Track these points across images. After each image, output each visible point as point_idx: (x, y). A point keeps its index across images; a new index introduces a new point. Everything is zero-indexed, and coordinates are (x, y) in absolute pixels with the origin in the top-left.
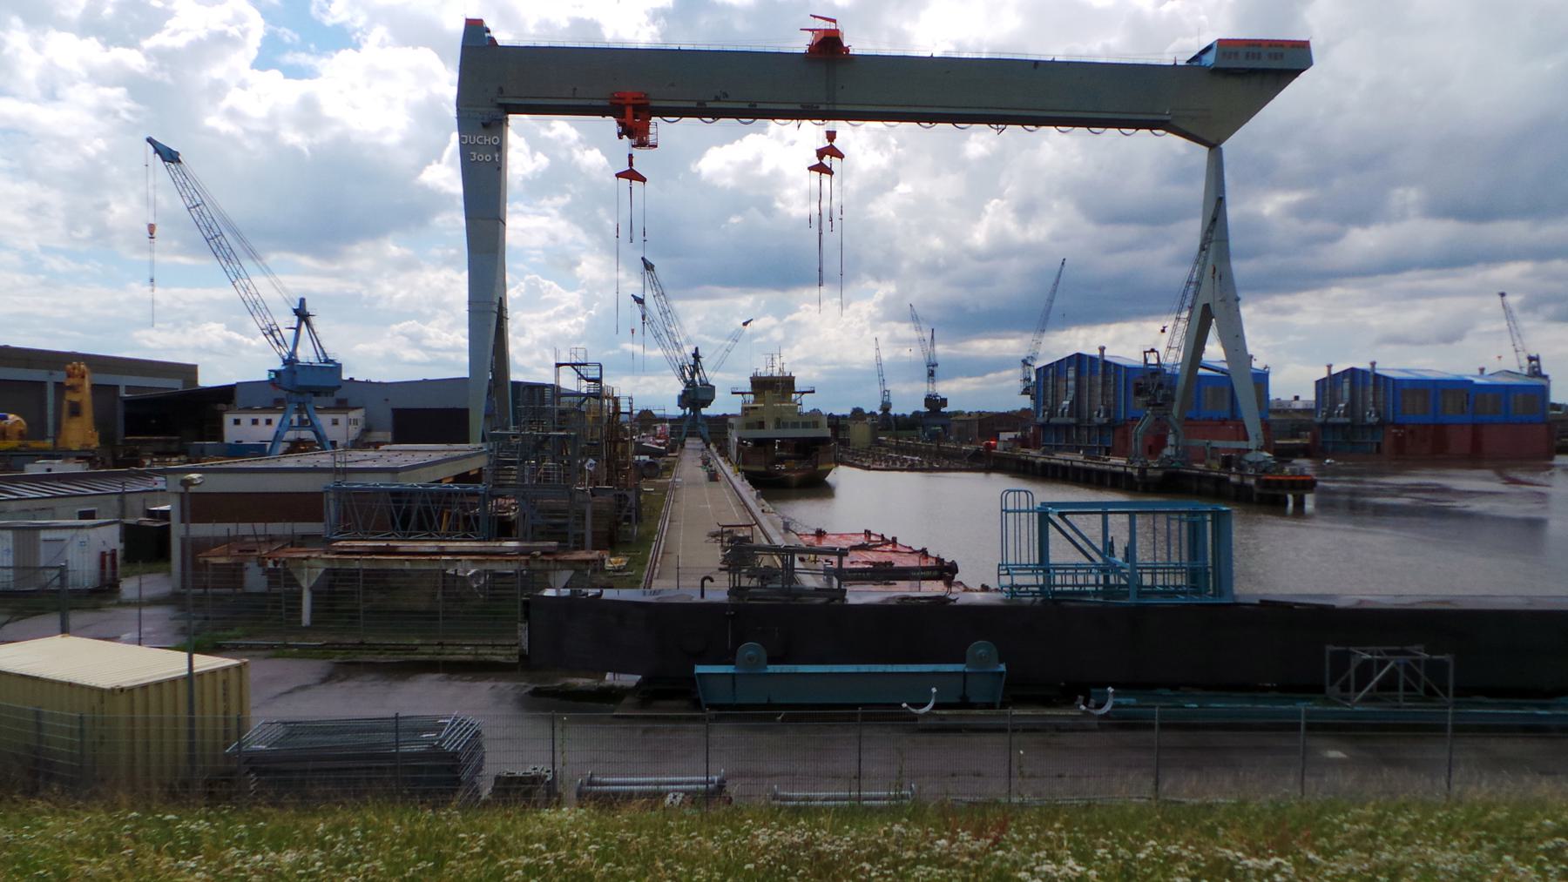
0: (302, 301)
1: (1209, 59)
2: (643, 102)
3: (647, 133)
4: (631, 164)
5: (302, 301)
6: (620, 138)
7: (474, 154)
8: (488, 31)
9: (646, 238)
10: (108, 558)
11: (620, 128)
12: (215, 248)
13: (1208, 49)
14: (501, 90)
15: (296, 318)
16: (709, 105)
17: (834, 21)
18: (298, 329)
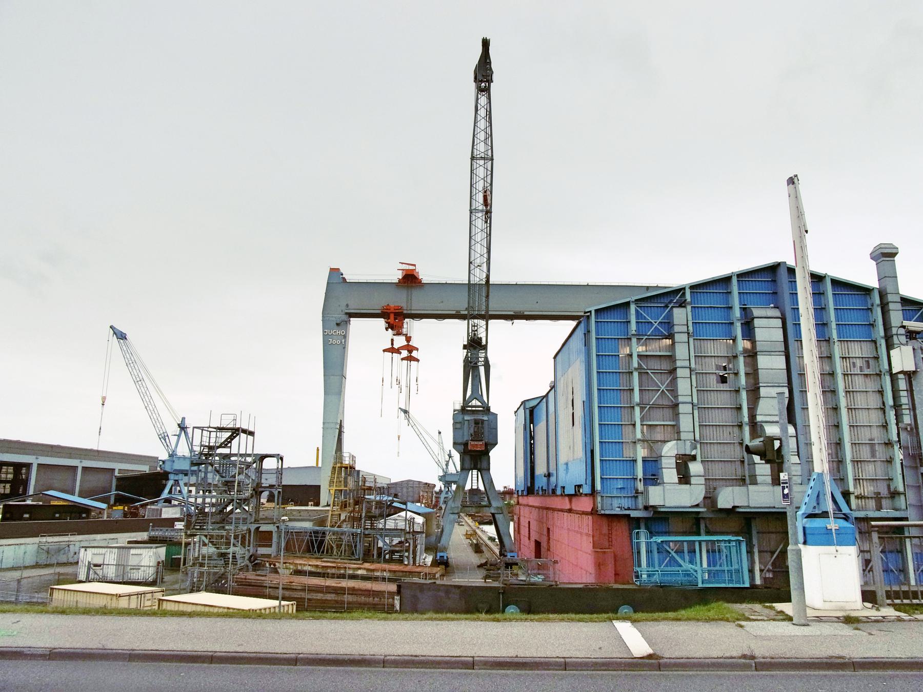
0: (183, 419)
2: (400, 311)
3: (402, 327)
4: (392, 344)
5: (183, 419)
6: (387, 330)
8: (342, 274)
12: (138, 387)
14: (347, 305)
15: (179, 429)
18: (179, 436)
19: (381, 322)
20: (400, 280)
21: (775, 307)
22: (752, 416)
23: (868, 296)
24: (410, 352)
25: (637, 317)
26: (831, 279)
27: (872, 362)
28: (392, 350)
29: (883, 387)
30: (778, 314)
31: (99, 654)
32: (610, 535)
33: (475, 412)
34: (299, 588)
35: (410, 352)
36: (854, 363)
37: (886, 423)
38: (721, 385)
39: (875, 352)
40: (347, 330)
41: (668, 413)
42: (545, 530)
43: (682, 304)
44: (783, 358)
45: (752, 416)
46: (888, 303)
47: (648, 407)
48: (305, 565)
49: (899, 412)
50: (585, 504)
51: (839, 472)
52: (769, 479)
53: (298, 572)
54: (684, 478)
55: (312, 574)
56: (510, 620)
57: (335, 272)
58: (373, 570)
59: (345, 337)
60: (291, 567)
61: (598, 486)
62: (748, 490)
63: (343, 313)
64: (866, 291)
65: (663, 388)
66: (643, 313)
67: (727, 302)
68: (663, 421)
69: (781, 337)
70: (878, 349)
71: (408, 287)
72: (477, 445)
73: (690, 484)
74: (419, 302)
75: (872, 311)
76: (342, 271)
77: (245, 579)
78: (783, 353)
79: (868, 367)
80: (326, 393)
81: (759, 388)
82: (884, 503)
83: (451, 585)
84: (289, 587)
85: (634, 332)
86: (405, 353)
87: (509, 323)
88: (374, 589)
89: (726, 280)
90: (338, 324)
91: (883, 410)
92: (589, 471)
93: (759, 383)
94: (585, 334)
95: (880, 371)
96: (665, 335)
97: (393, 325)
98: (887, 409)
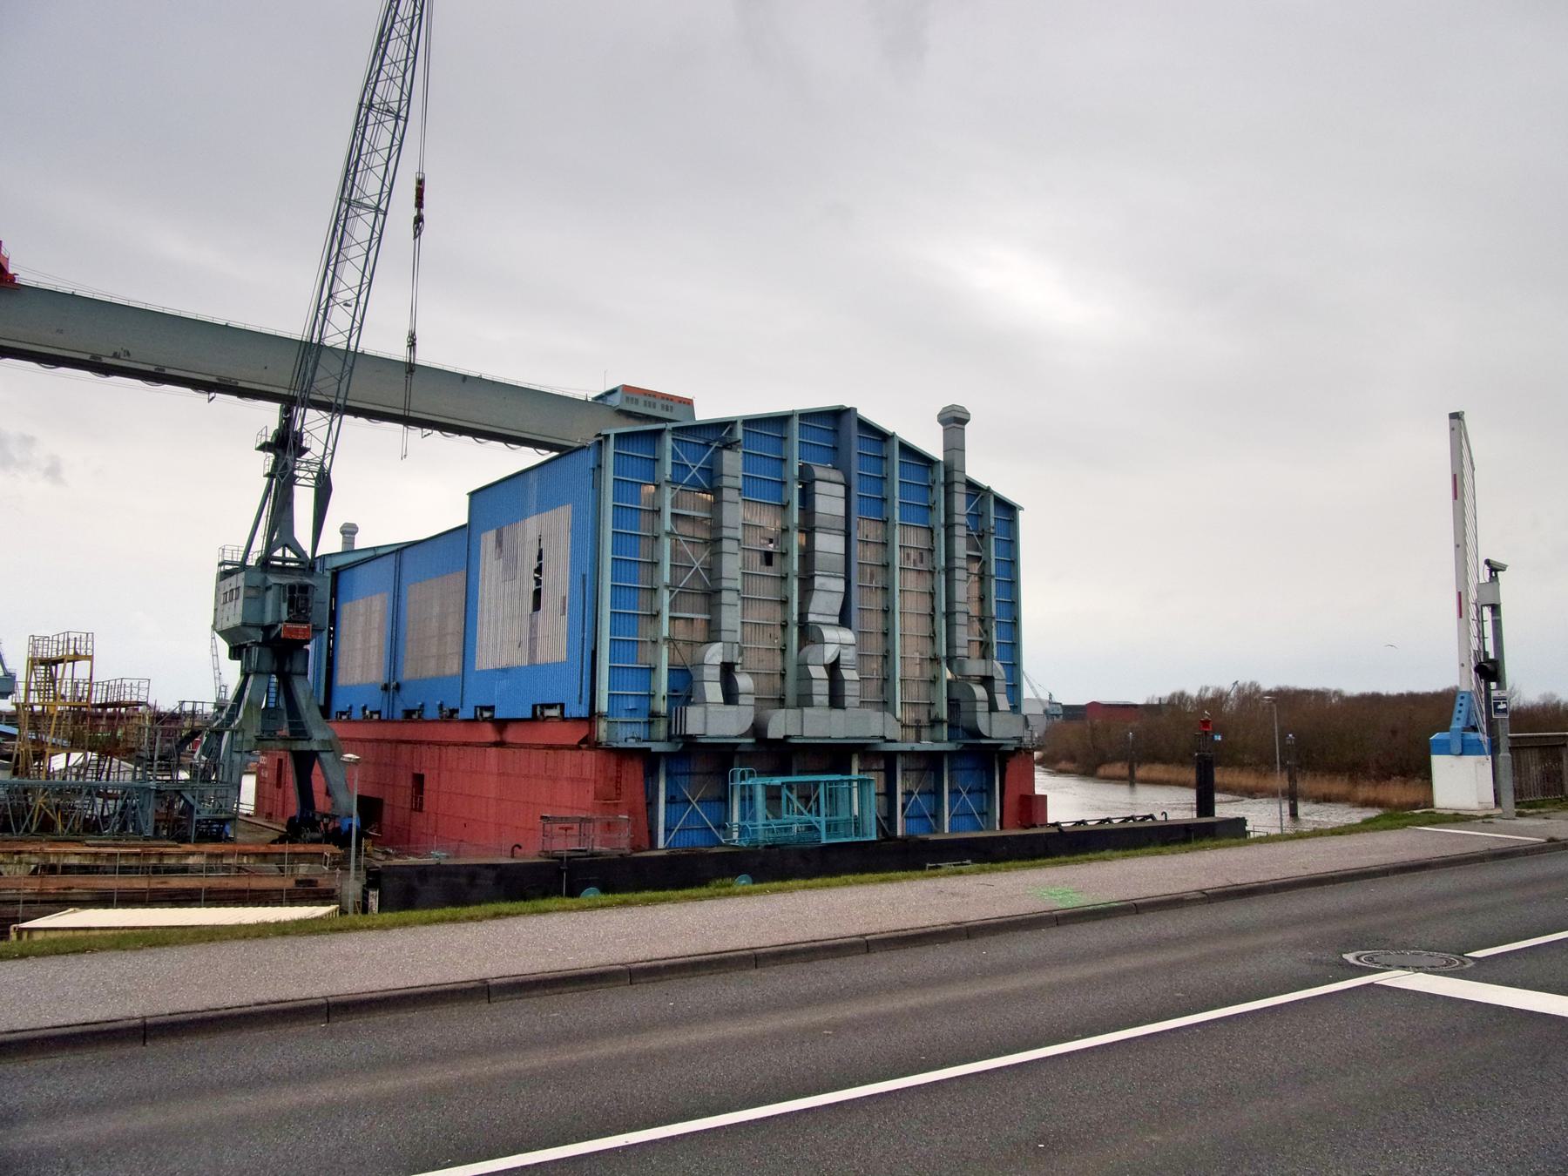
1: (615, 401)
21: (834, 468)
22: (803, 615)
25: (673, 454)
26: (900, 442)
29: (935, 587)
30: (841, 478)
31: (845, 944)
32: (618, 782)
33: (287, 571)
34: (87, 897)
36: (908, 555)
37: (934, 633)
38: (766, 568)
43: (729, 444)
45: (803, 615)
46: (953, 483)
47: (678, 590)
48: (66, 854)
50: (572, 735)
52: (826, 700)
54: (730, 696)
56: (738, 895)
57: (1503, 568)
60: (35, 859)
61: (603, 705)
62: (802, 715)
64: (928, 462)
65: (697, 565)
66: (681, 454)
67: (780, 451)
69: (842, 512)
70: (935, 539)
73: (844, 708)
79: (922, 561)
81: (813, 577)
82: (925, 733)
83: (478, 865)
84: (61, 898)
85: (668, 477)
87: (200, 398)
89: (781, 420)
93: (814, 570)
94: (594, 469)
95: (934, 568)
96: (702, 487)
98: (937, 618)
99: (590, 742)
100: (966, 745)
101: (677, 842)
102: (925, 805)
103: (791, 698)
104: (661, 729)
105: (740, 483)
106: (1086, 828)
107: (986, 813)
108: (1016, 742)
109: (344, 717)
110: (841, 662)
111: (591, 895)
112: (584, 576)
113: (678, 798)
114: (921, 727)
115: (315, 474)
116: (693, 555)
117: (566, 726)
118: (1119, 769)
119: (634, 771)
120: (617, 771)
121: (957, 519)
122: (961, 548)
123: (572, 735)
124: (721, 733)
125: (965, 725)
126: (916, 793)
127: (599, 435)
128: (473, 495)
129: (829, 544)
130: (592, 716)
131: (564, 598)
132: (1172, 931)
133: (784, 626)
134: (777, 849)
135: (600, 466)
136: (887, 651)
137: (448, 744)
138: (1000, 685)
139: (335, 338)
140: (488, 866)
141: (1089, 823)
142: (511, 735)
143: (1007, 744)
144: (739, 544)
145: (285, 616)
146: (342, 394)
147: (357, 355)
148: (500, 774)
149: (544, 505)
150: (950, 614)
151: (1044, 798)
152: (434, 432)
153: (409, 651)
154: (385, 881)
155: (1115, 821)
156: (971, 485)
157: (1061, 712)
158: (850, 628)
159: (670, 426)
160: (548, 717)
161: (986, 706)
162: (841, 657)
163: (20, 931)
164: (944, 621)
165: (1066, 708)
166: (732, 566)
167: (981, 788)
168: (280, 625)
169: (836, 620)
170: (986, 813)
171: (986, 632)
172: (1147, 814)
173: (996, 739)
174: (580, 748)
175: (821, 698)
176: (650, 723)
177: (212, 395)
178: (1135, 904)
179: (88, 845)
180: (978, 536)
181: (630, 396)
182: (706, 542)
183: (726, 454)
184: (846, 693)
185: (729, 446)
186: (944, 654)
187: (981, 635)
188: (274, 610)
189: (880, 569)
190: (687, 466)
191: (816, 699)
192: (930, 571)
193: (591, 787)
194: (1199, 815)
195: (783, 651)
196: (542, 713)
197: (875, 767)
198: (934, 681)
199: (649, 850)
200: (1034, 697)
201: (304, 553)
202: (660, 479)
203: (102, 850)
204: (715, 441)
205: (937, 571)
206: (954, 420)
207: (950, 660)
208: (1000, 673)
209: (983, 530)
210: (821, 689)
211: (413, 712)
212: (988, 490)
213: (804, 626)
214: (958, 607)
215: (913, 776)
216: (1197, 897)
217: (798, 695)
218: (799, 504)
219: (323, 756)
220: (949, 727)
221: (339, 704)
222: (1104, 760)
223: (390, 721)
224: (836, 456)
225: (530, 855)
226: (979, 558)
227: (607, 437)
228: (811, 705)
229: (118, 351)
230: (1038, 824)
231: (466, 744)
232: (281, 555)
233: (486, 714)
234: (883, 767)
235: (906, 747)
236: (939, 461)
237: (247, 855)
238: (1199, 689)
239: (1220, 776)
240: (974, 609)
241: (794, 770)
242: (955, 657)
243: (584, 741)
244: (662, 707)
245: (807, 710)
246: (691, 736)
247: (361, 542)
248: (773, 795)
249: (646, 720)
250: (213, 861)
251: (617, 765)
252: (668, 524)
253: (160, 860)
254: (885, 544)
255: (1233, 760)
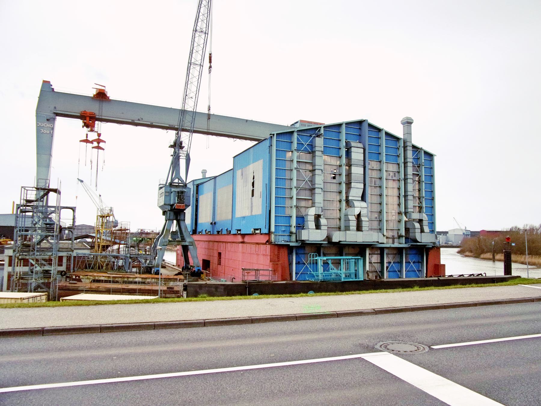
2: (94, 116)
3: (94, 126)
4: (87, 137)
7: (42, 130)
8: (52, 86)
9: (105, 164)
10: (19, 265)
11: (83, 124)
13: (297, 122)
14: (55, 108)
16: (136, 122)
17: (105, 87)
19: (80, 122)
20: (94, 95)
22: (347, 197)
23: (398, 142)
24: (99, 143)
25: (298, 141)
26: (385, 132)
27: (396, 174)
28: (87, 141)
34: (104, 290)
35: (99, 143)
36: (389, 174)
38: (333, 180)
39: (398, 170)
40: (54, 124)
41: (308, 192)
42: (216, 255)
43: (318, 135)
44: (363, 169)
45: (347, 197)
46: (407, 146)
49: (406, 199)
50: (264, 239)
51: (379, 226)
52: (355, 228)
53: (95, 281)
54: (318, 226)
55: (106, 281)
57: (46, 84)
58: (146, 278)
59: (53, 129)
60: (91, 278)
61: (273, 229)
63: (52, 112)
64: (397, 139)
65: (307, 179)
66: (301, 140)
67: (339, 137)
68: (305, 197)
71: (100, 100)
72: (180, 206)
73: (362, 231)
74: (106, 111)
75: (399, 149)
76: (51, 83)
77: (66, 286)
78: (363, 166)
80: (38, 165)
81: (351, 183)
82: (396, 240)
84: (97, 290)
85: (295, 148)
86: (95, 144)
88: (153, 289)
89: (340, 125)
90: (48, 120)
91: (399, 197)
92: (268, 221)
93: (351, 180)
94: (269, 146)
95: (400, 179)
97: (88, 124)
98: (401, 197)
99: (269, 242)
100: (412, 245)
101: (301, 278)
102: (396, 267)
103: (343, 228)
104: (293, 238)
105: (322, 149)
106: (463, 278)
107: (421, 271)
108: (431, 244)
109: (200, 233)
110: (361, 214)
111: (311, 293)
112: (266, 184)
113: (301, 262)
114: (395, 238)
115: (185, 155)
116: (305, 176)
117: (262, 236)
118: (489, 255)
119: (284, 253)
120: (278, 252)
121: (408, 160)
122: (410, 171)
123: (264, 239)
124: (315, 240)
125: (411, 238)
126: (392, 262)
127: (271, 134)
128: (234, 157)
129: (357, 171)
130: (269, 233)
131: (261, 192)
132: (177, 337)
133: (340, 201)
134: (325, 283)
135: (271, 145)
136: (381, 210)
137: (228, 242)
138: (425, 223)
139: (189, 107)
140: (222, 285)
141: (454, 276)
142: (247, 239)
143: (429, 245)
144: (322, 172)
145: (177, 202)
146: (192, 127)
147: (196, 113)
148: (243, 253)
149: (255, 160)
150: (406, 196)
151: (444, 265)
152: (237, 139)
153: (218, 211)
154: (188, 289)
155: (465, 276)
156: (414, 147)
157: (470, 234)
158: (365, 202)
159: (296, 130)
160: (257, 233)
161: (419, 230)
162: (361, 213)
163: (63, 300)
164: (403, 199)
165: (471, 232)
166: (319, 180)
167: (419, 261)
168: (175, 204)
169: (360, 199)
170: (421, 271)
171: (421, 202)
172: (479, 273)
173: (424, 243)
174: (266, 244)
175: (353, 227)
176: (290, 236)
177: (168, 130)
178: (337, 313)
179: (108, 274)
180: (418, 166)
181: (303, 124)
182: (310, 171)
183: (317, 139)
184: (363, 225)
185: (318, 136)
186: (404, 211)
187: (419, 204)
188: (174, 199)
189: (378, 180)
190: (303, 144)
191: (351, 228)
192: (398, 180)
193: (269, 257)
194: (505, 274)
195: (340, 210)
196: (255, 232)
197: (376, 253)
198: (399, 221)
199: (280, 281)
200: (459, 228)
201: (183, 180)
202: (293, 149)
203: (111, 275)
204: (313, 134)
205: (401, 180)
206: (408, 123)
207: (406, 213)
208: (425, 218)
209: (420, 164)
210: (353, 224)
211: (220, 232)
212: (421, 149)
213: (347, 201)
214: (409, 193)
215: (391, 257)
216: (372, 311)
217: (345, 226)
218: (346, 156)
219: (190, 247)
220: (405, 238)
221: (199, 230)
222: (483, 252)
223: (213, 235)
224: (360, 137)
225: (238, 281)
226: (418, 175)
227: (274, 135)
228: (349, 230)
229: (140, 118)
230: (442, 276)
231: (233, 242)
232: (177, 182)
233: (239, 232)
234: (379, 253)
235: (388, 246)
236: (401, 139)
237: (154, 278)
238: (523, 225)
239: (513, 257)
240: (417, 194)
241: (344, 253)
242: (408, 212)
243: (267, 241)
244: (294, 230)
245: (347, 232)
246: (303, 240)
247: (208, 175)
248: (325, 263)
249: (289, 234)
250: (144, 280)
251: (278, 250)
252: (295, 165)
253: (128, 279)
254: (380, 170)
255: (521, 252)
